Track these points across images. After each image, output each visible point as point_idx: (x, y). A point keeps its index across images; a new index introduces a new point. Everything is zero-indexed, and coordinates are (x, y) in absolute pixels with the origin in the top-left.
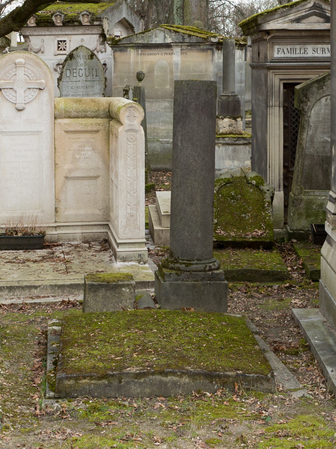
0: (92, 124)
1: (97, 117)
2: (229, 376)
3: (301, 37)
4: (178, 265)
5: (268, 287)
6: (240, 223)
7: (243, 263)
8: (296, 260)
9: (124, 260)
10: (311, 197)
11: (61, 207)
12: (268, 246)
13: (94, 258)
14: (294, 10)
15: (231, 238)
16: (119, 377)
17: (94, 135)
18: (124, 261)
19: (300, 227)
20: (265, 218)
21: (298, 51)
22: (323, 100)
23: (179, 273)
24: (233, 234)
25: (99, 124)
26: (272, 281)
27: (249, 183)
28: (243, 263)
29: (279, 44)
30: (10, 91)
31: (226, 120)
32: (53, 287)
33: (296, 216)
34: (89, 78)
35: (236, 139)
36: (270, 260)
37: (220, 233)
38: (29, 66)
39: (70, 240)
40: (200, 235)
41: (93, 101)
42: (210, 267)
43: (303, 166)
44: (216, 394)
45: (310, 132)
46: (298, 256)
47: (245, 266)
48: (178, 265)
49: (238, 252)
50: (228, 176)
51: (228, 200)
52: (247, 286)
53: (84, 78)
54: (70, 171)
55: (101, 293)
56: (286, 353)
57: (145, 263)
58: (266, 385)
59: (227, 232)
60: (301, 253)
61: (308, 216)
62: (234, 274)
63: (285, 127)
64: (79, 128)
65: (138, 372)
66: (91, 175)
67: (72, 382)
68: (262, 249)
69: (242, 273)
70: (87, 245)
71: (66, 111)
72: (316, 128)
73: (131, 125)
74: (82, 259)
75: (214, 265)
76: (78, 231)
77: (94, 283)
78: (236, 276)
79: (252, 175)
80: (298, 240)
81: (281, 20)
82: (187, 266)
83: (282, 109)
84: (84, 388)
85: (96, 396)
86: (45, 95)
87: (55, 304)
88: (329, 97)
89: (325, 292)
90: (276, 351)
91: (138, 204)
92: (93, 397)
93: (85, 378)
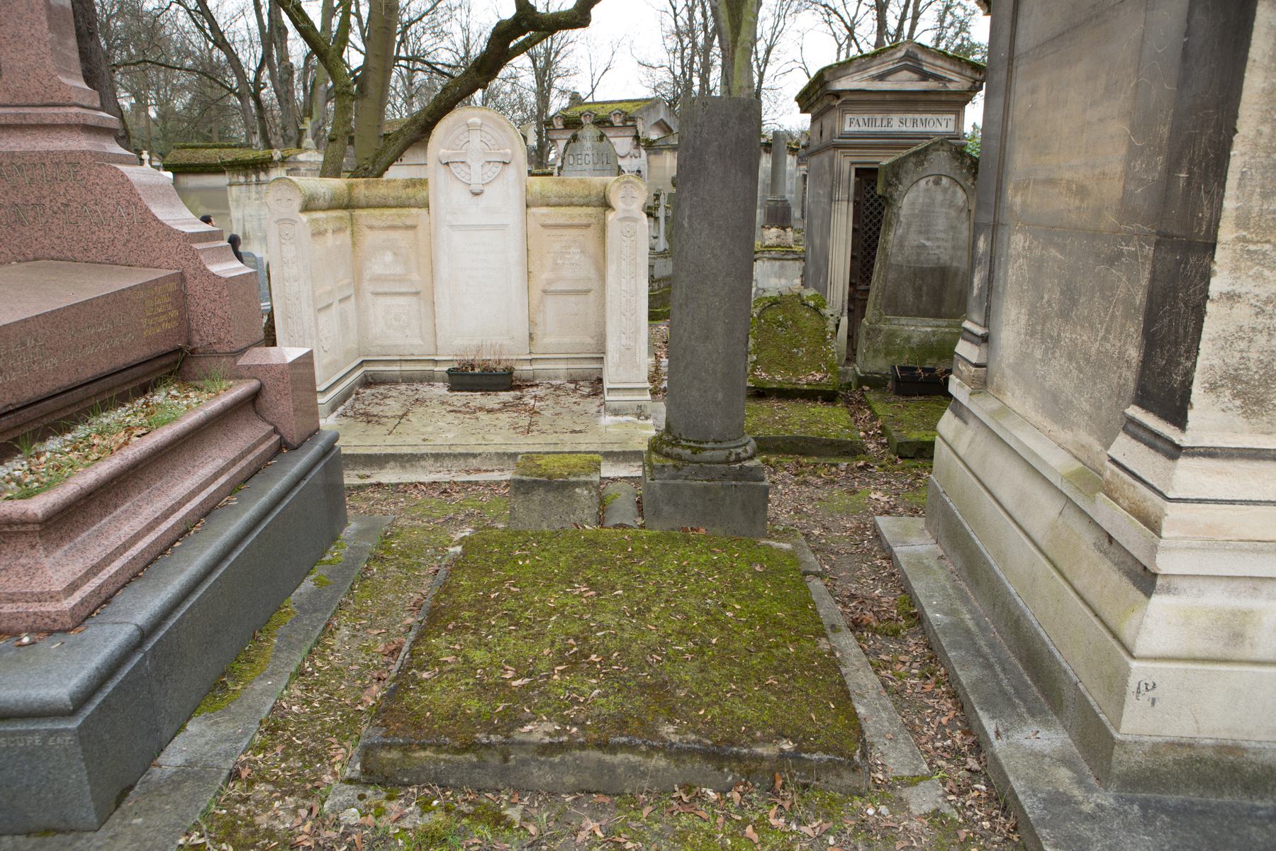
1: (587, 205)
2: (761, 758)
3: (884, 102)
4: (678, 450)
5: (832, 465)
7: (793, 424)
8: (871, 420)
9: (616, 413)
10: (895, 327)
11: (538, 332)
12: (829, 397)
13: (575, 408)
16: (502, 750)
17: (584, 232)
18: (616, 415)
19: (875, 369)
20: (826, 355)
21: (878, 123)
22: (923, 182)
23: (680, 464)
24: (778, 378)
25: (590, 215)
26: (837, 456)
28: (793, 424)
30: (462, 166)
31: (773, 230)
32: (500, 456)
33: (871, 353)
34: (598, 167)
35: (784, 253)
36: (832, 421)
38: (487, 129)
39: (550, 378)
40: (720, 396)
41: (581, 181)
42: (738, 454)
43: (885, 281)
44: (728, 795)
45: (900, 232)
46: (873, 412)
47: (796, 431)
48: (678, 450)
49: (785, 404)
50: (775, 294)
52: (798, 462)
53: (591, 166)
54: (550, 282)
55: (538, 496)
56: (875, 631)
57: (647, 418)
58: (848, 779)
60: (879, 408)
61: (888, 354)
63: (854, 230)
64: (562, 221)
65: (547, 740)
66: (580, 288)
67: (395, 754)
70: (573, 386)
71: (543, 197)
72: (909, 225)
73: (627, 211)
74: (558, 409)
75: (746, 451)
76: (562, 366)
77: (524, 478)
79: (809, 293)
81: (857, 77)
82: (694, 453)
83: (851, 205)
84: (424, 768)
85: (451, 786)
86: (511, 172)
87: (498, 483)
88: (932, 179)
89: (944, 503)
90: (856, 626)
91: (637, 331)
92: (444, 787)
93: (423, 747)
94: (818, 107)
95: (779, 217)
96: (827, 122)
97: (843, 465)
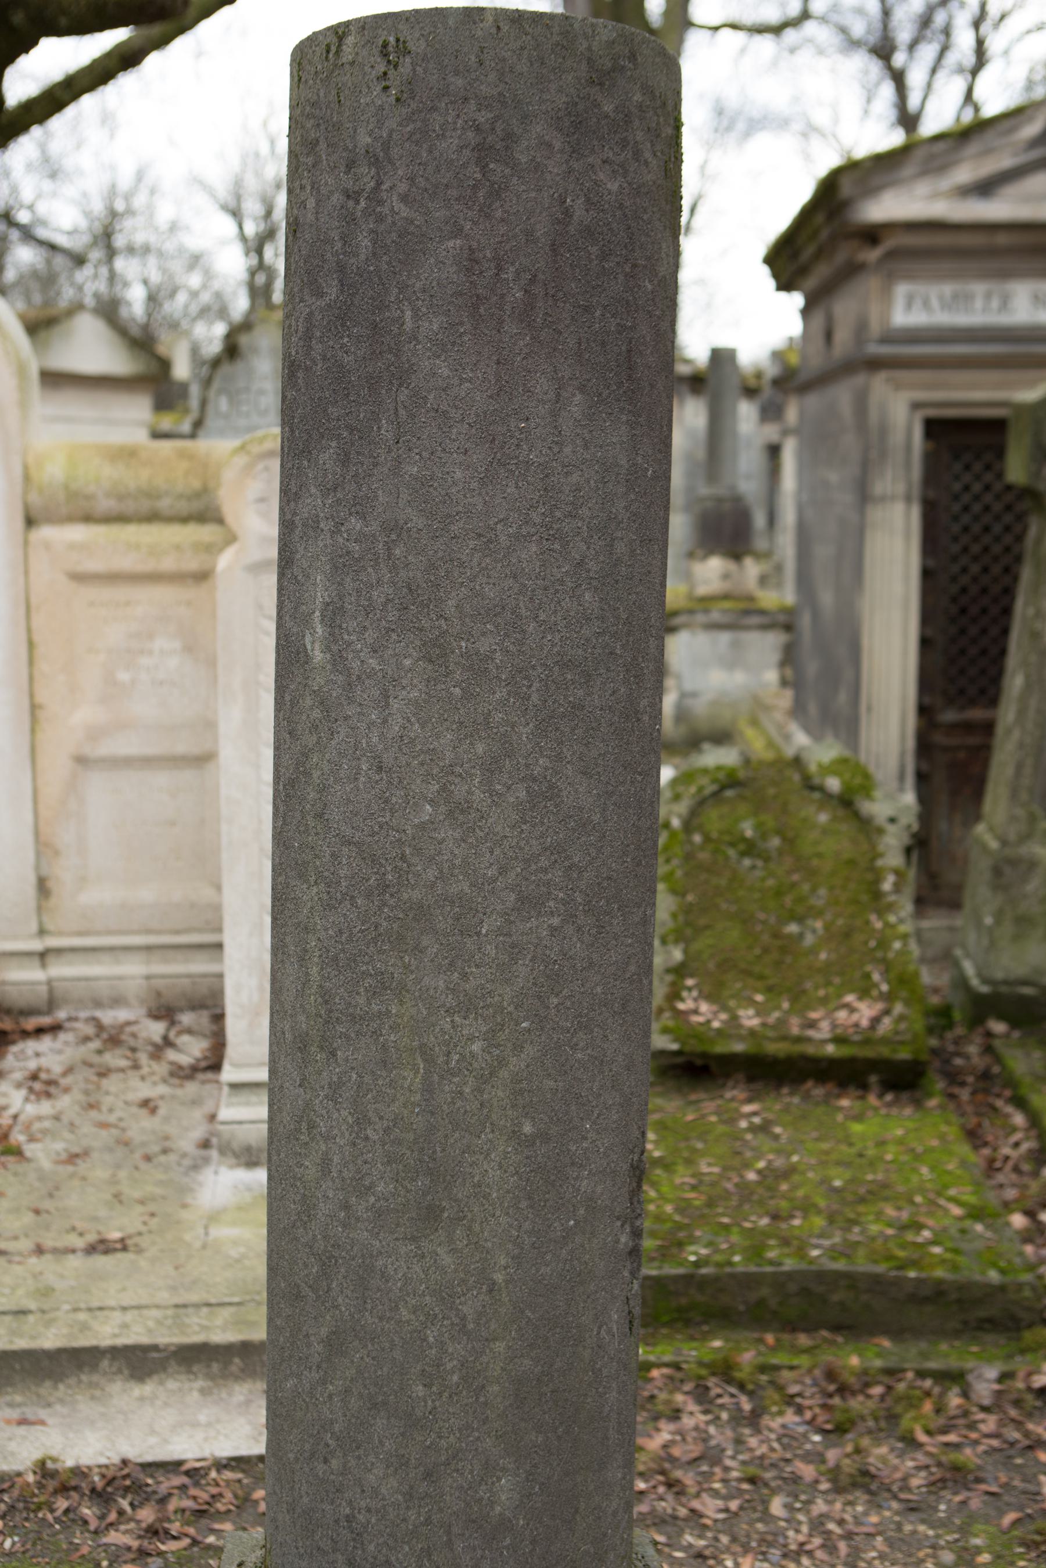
0: (178, 548)
6: (778, 964)
11: (63, 874)
12: (900, 1079)
14: (973, 147)
15: (741, 1038)
19: (1020, 971)
20: (883, 944)
21: (979, 304)
24: (749, 1019)
27: (812, 788)
29: (910, 277)
35: (739, 614)
37: (696, 1012)
39: (98, 1004)
40: (505, 1491)
51: (727, 858)
52: (831, 1375)
54: (95, 733)
59: (724, 1008)
62: (765, 1291)
64: (127, 563)
66: (181, 748)
68: (875, 1088)
69: (805, 1292)
70: (156, 1029)
71: (73, 495)
78: (773, 1303)
80: (1014, 1023)
81: (923, 188)
94: (821, 272)
95: (728, 530)
96: (844, 309)
97: (985, 1381)
